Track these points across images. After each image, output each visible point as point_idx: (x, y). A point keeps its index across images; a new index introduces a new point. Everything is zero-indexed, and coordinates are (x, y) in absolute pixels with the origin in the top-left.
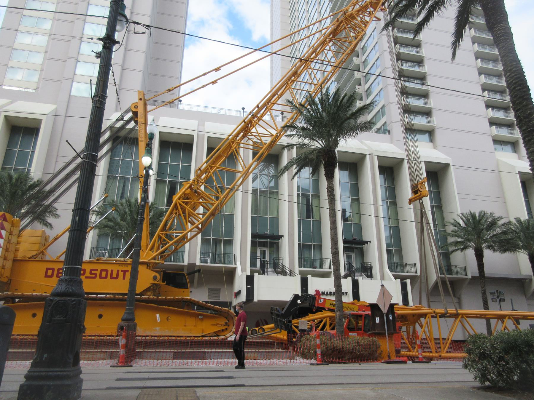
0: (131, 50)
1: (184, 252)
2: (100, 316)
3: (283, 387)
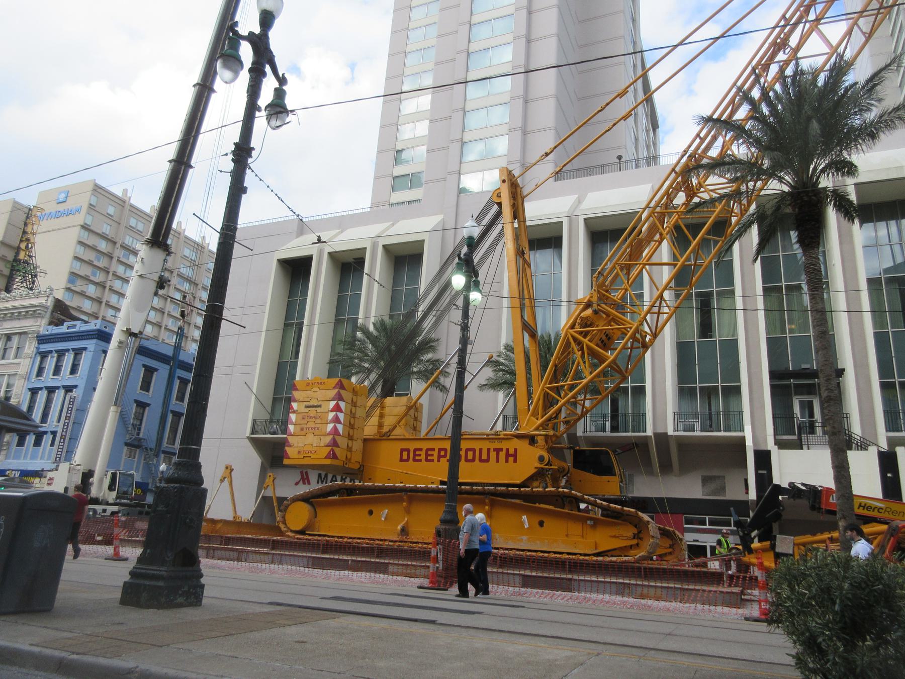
0: (536, 100)
1: (741, 413)
2: (371, 513)
3: (559, 640)
